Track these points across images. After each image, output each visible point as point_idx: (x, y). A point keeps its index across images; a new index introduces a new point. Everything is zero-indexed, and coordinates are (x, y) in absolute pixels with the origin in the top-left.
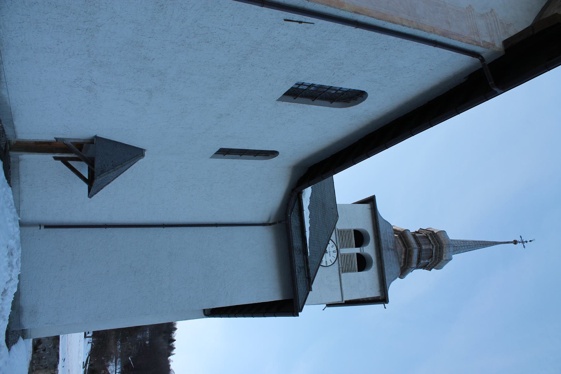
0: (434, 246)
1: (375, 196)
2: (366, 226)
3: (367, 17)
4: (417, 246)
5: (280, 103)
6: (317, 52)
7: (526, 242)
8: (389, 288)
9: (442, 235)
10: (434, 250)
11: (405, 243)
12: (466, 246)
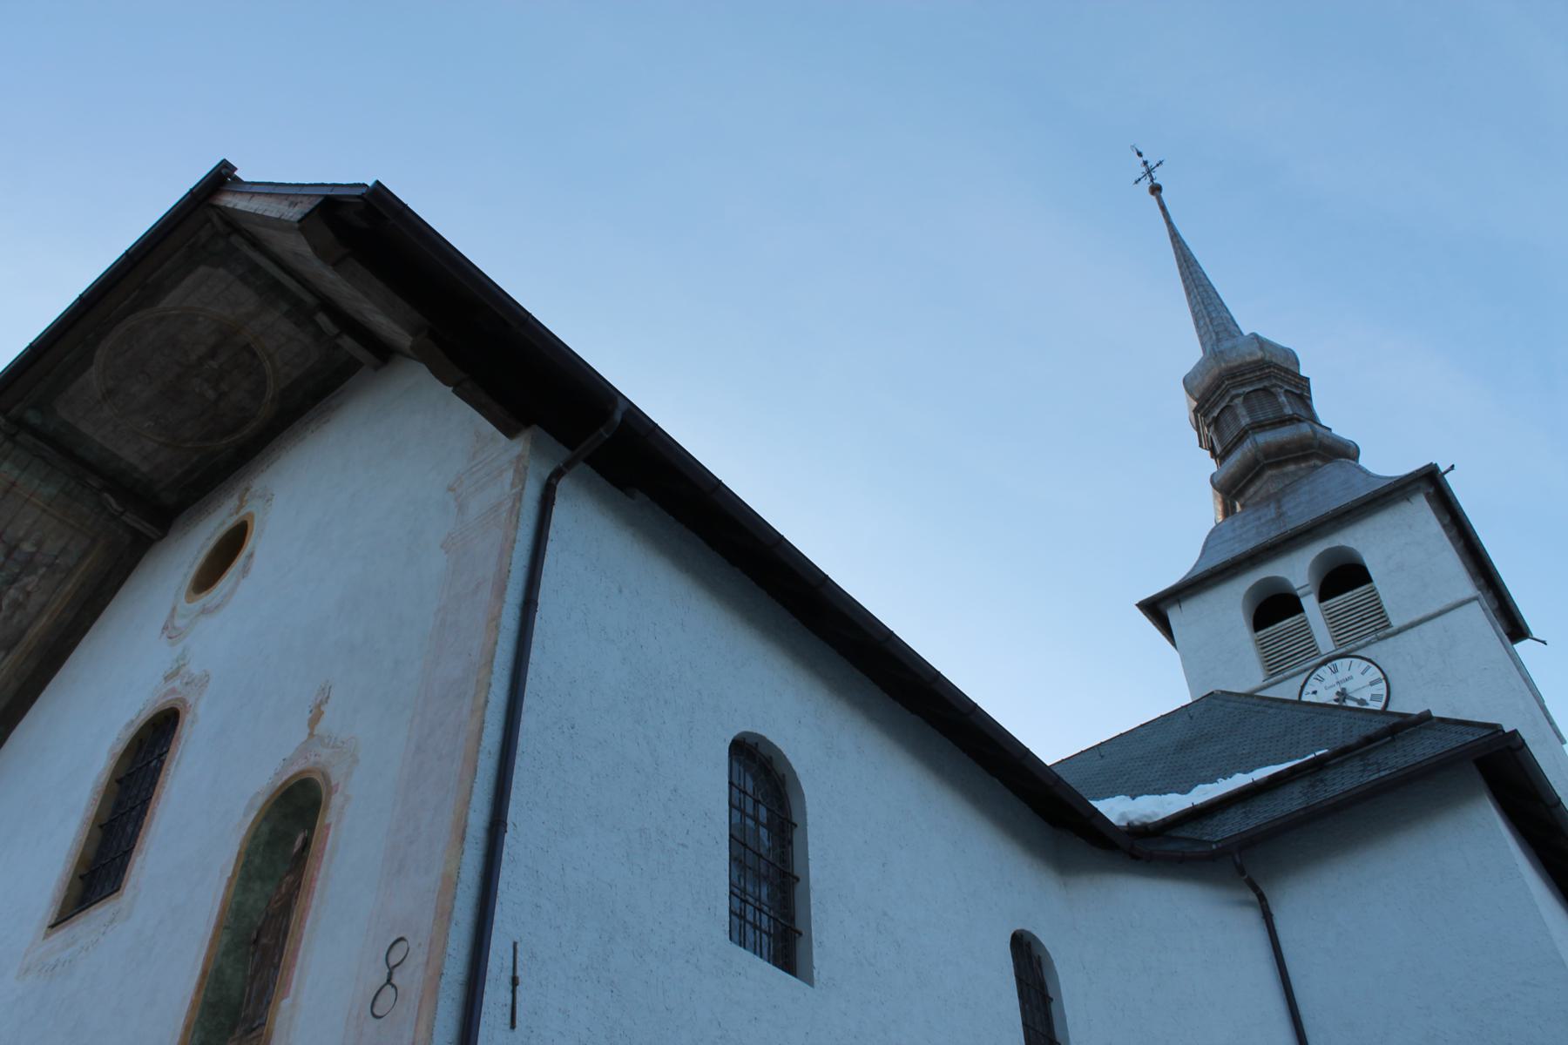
0: (1234, 392)
1: (1137, 602)
2: (1231, 601)
3: (471, 806)
4: (1248, 441)
5: (819, 973)
6: (612, 912)
7: (1145, 163)
8: (1391, 478)
9: (1196, 383)
10: (1244, 389)
11: (1250, 476)
12: (1206, 308)
